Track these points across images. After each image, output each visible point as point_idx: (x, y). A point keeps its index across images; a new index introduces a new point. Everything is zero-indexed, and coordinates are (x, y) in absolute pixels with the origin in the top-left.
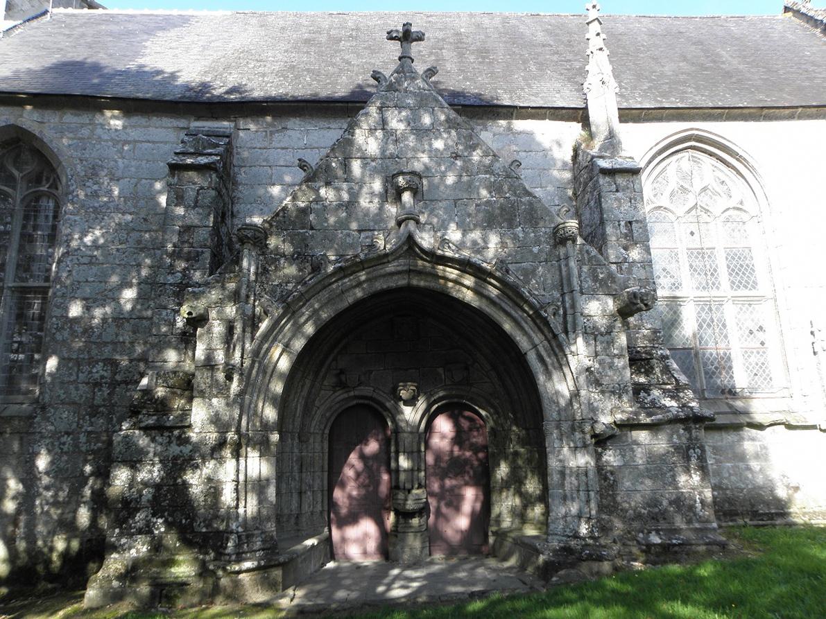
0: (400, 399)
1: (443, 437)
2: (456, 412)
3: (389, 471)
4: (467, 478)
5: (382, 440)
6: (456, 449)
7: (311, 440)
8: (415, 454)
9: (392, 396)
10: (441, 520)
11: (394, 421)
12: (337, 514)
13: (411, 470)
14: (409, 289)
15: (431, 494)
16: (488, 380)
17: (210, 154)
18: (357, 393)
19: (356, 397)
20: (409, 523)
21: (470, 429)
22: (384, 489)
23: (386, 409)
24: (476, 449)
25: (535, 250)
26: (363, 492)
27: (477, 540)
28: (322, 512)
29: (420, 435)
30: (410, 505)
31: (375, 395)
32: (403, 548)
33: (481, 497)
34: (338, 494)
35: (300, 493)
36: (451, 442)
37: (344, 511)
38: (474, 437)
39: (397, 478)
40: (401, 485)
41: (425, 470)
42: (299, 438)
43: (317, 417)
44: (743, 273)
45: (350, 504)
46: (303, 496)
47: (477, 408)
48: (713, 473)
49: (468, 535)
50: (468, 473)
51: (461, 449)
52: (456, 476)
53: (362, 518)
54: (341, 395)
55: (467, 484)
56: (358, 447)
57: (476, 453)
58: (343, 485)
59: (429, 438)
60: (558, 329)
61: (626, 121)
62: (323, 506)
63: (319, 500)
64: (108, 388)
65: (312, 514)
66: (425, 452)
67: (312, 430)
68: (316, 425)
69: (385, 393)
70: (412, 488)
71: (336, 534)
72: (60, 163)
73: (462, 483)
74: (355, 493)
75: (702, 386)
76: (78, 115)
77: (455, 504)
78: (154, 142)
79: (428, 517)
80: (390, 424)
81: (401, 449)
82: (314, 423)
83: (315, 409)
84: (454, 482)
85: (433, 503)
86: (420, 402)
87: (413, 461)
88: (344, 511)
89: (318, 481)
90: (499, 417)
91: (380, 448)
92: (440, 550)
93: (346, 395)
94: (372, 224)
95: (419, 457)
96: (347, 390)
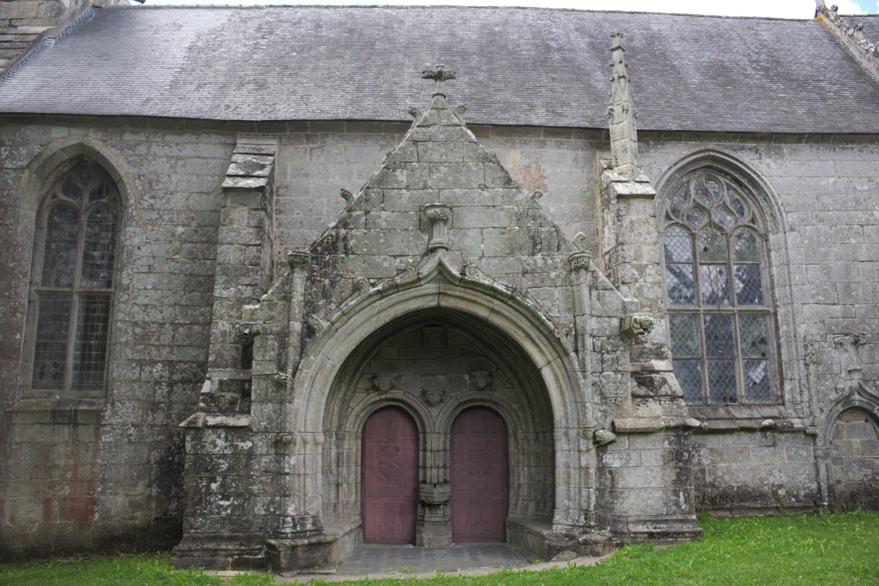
14: (438, 308)
16: (510, 386)
17: (259, 177)
18: (388, 396)
25: (553, 274)
31: (405, 398)
35: (338, 485)
40: (428, 480)
42: (337, 436)
44: (751, 288)
46: (340, 488)
48: (709, 472)
54: (374, 397)
60: (570, 347)
63: (354, 491)
64: (168, 386)
68: (353, 426)
72: (121, 179)
75: (705, 394)
76: (136, 133)
78: (203, 158)
82: (349, 422)
83: (350, 409)
89: (353, 476)
93: (378, 398)
94: (406, 250)
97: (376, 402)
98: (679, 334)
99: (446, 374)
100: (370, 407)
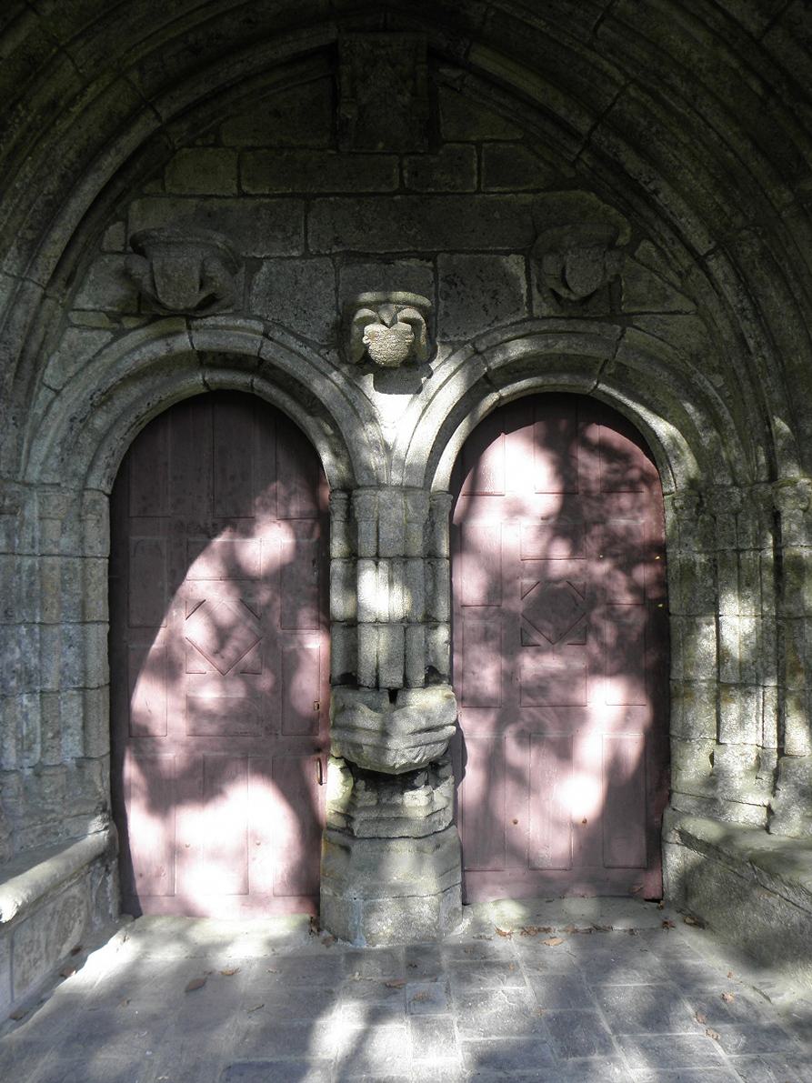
0: (365, 362)
1: (516, 511)
2: (563, 424)
3: (326, 622)
4: (594, 648)
5: (302, 516)
6: (560, 551)
7: (32, 510)
8: (418, 565)
9: (333, 356)
10: (507, 791)
11: (344, 448)
12: (148, 763)
13: (404, 625)
15: (473, 702)
16: (690, 306)
18: (202, 340)
19: (204, 359)
20: (397, 807)
21: (611, 488)
22: (310, 686)
23: (316, 407)
24: (626, 553)
26: (238, 691)
27: (628, 852)
28: (83, 762)
29: (433, 497)
30: (402, 752)
31: (270, 352)
32: (371, 893)
33: (644, 713)
34: (149, 698)
36: (542, 529)
37: (172, 756)
38: (621, 511)
39: (353, 650)
40: (366, 676)
41: (450, 622)
43: (55, 428)
45: (194, 733)
47: (641, 410)
49: (594, 838)
50: (597, 631)
51: (576, 550)
52: (557, 640)
53: (232, 779)
54: (142, 346)
55: (596, 670)
56: (219, 541)
57: (19, 661)
58: (170, 670)
59: (468, 513)
61: (139, 909)
62: (85, 744)
65: (38, 775)
66: (450, 558)
67: (34, 474)
69: (306, 342)
70: (407, 685)
71: (144, 832)
73: (580, 664)
74: (209, 695)
77: (553, 733)
79: (459, 775)
80: (326, 458)
81: (367, 547)
82: (41, 449)
83: (43, 395)
84: (552, 663)
85: (477, 730)
86: (438, 378)
87: (408, 584)
88: (172, 756)
90: (722, 442)
91: (297, 547)
92: (504, 883)
93: (159, 349)
95: (433, 575)
96: (163, 326)
97: (157, 367)
98: (759, 381)
99: (431, 257)
100: (135, 390)
